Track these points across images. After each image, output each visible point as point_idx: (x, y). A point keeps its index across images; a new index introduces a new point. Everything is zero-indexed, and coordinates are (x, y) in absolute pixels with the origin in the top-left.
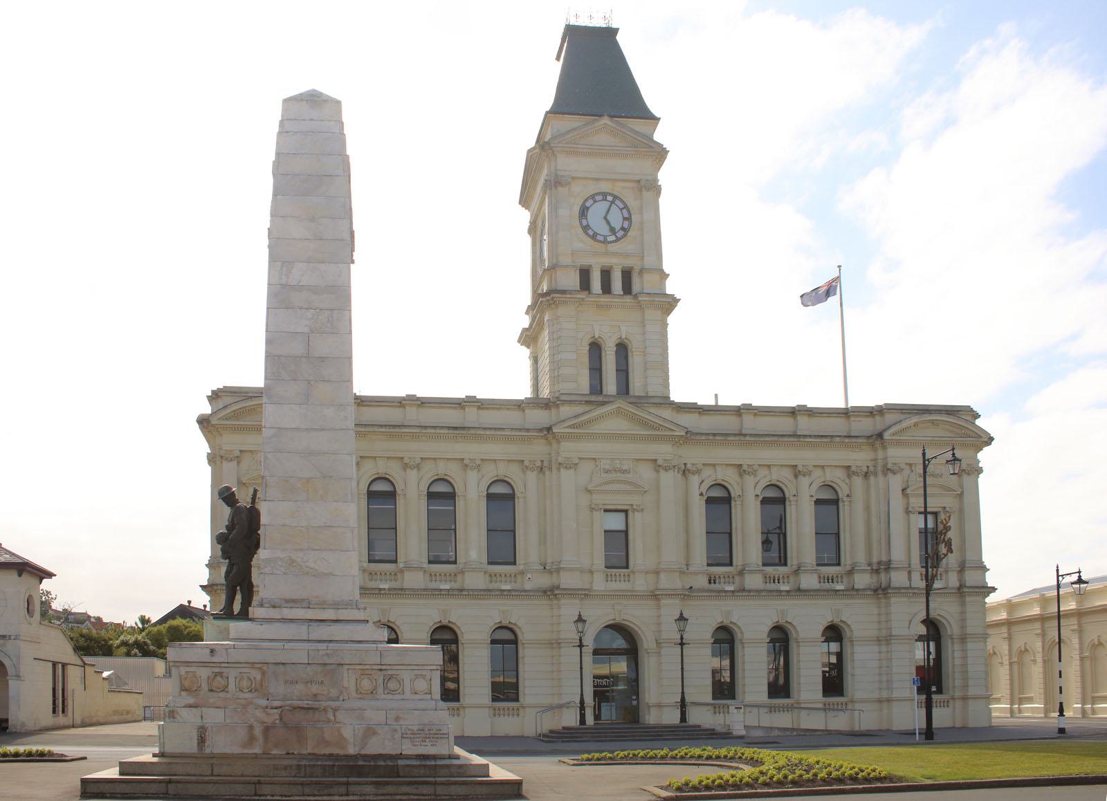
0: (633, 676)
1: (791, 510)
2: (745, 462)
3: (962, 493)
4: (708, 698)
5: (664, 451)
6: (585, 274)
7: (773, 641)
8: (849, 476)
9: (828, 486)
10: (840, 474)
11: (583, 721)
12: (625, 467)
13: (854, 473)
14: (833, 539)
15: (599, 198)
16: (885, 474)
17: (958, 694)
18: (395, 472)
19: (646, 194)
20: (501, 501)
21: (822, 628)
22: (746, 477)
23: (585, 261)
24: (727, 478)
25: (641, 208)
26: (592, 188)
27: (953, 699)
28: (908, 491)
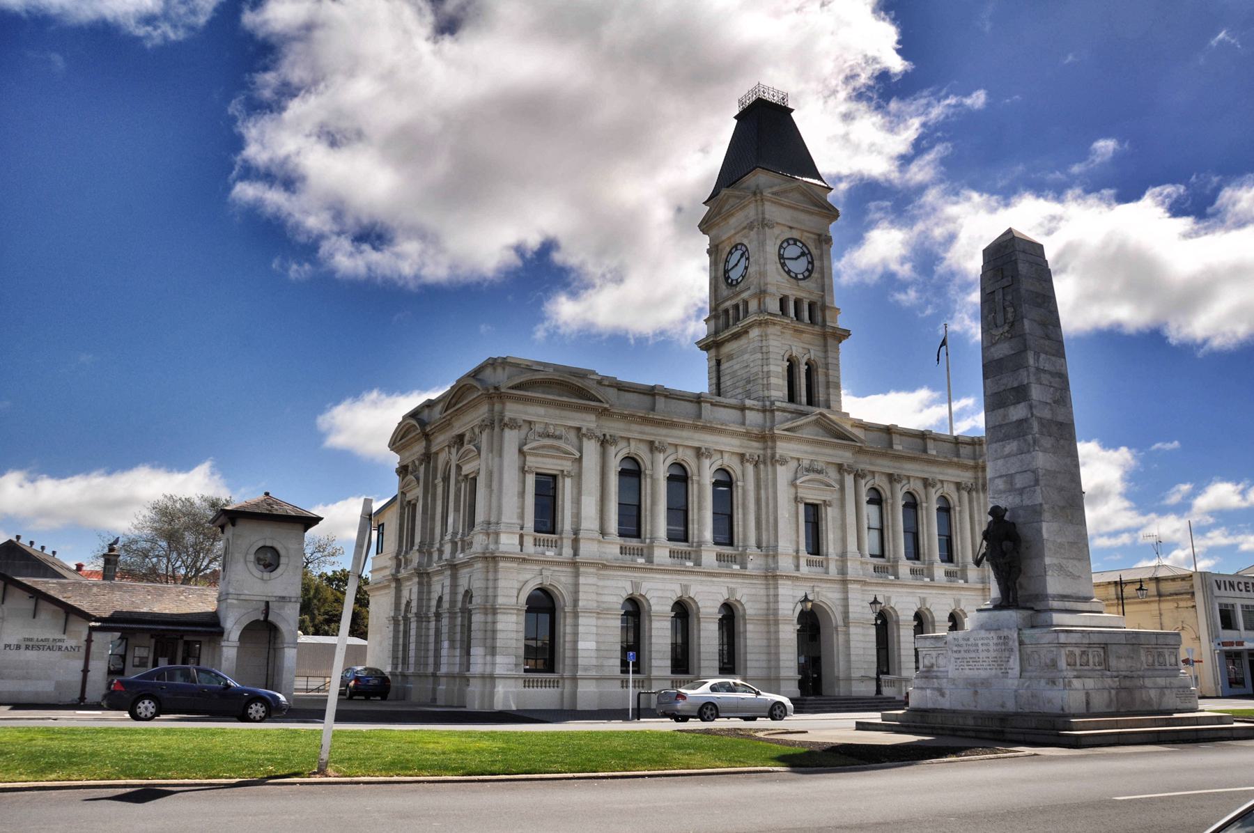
0: (154, 634)
1: (693, 489)
2: (657, 440)
3: (581, 457)
4: (668, 672)
5: (846, 457)
6: (783, 302)
7: (626, 614)
8: (742, 462)
9: (722, 470)
10: (953, 487)
11: (297, 690)
12: (557, 433)
13: (584, 435)
14: (681, 514)
15: (785, 245)
16: (773, 465)
17: (567, 674)
18: (643, 454)
19: (825, 247)
20: (725, 484)
21: (672, 603)
22: (657, 454)
23: (787, 292)
24: (686, 458)
25: (822, 255)
26: (788, 235)
27: (563, 678)
28: (525, 448)
